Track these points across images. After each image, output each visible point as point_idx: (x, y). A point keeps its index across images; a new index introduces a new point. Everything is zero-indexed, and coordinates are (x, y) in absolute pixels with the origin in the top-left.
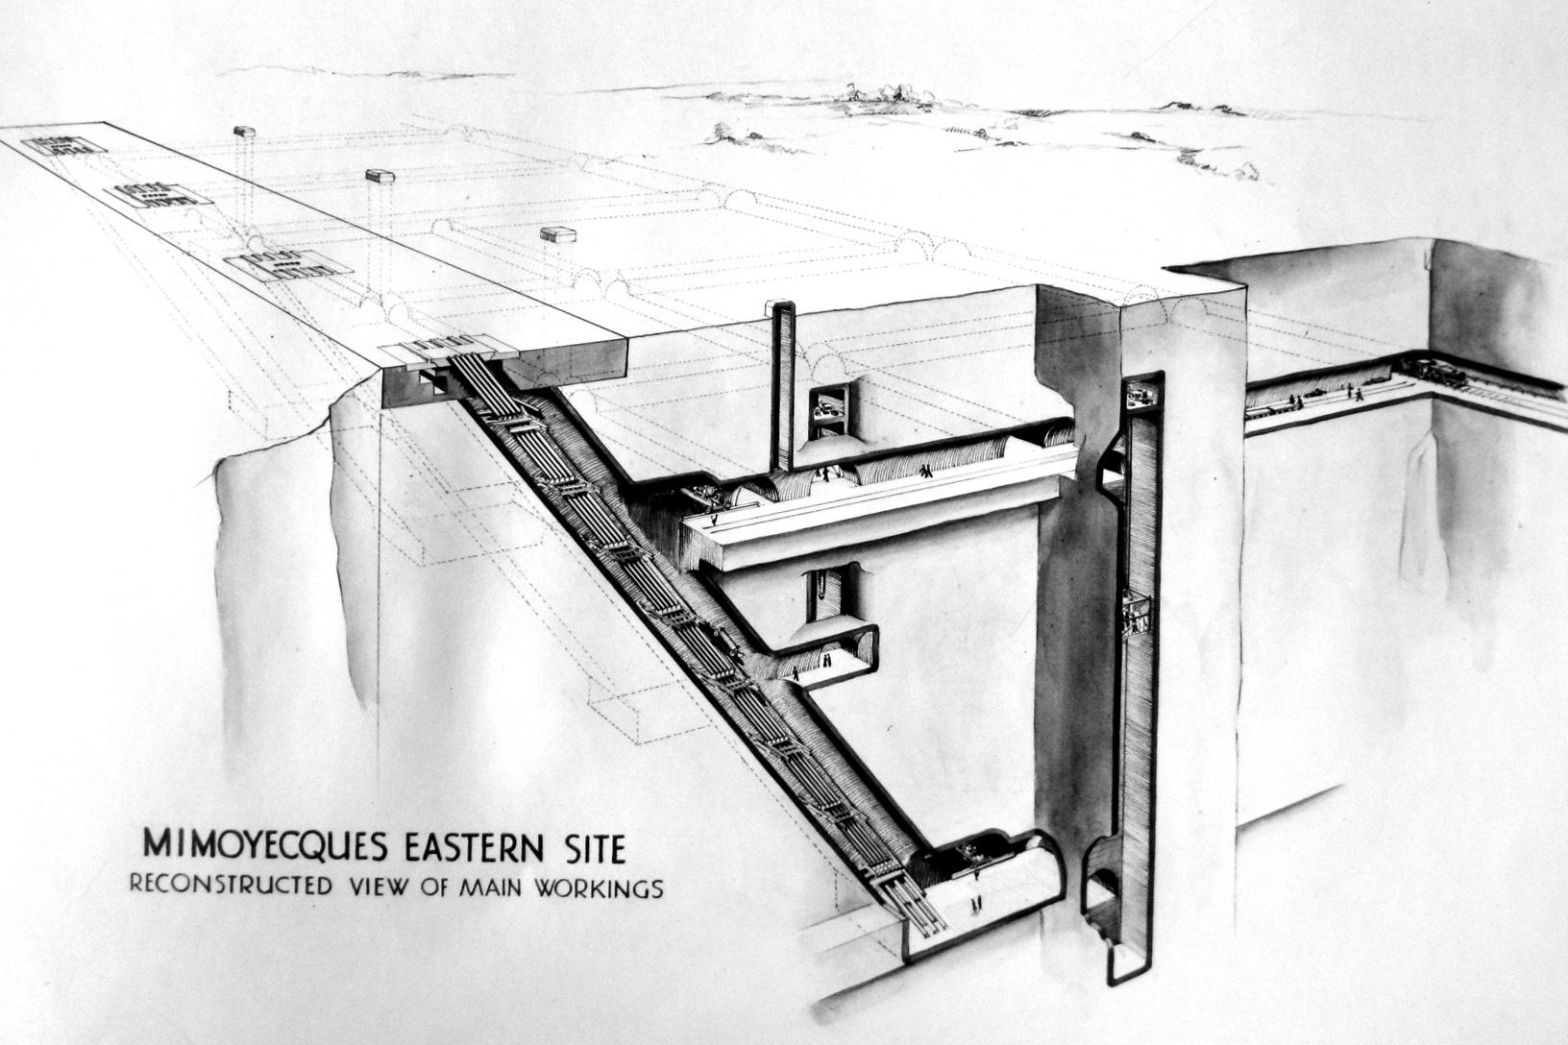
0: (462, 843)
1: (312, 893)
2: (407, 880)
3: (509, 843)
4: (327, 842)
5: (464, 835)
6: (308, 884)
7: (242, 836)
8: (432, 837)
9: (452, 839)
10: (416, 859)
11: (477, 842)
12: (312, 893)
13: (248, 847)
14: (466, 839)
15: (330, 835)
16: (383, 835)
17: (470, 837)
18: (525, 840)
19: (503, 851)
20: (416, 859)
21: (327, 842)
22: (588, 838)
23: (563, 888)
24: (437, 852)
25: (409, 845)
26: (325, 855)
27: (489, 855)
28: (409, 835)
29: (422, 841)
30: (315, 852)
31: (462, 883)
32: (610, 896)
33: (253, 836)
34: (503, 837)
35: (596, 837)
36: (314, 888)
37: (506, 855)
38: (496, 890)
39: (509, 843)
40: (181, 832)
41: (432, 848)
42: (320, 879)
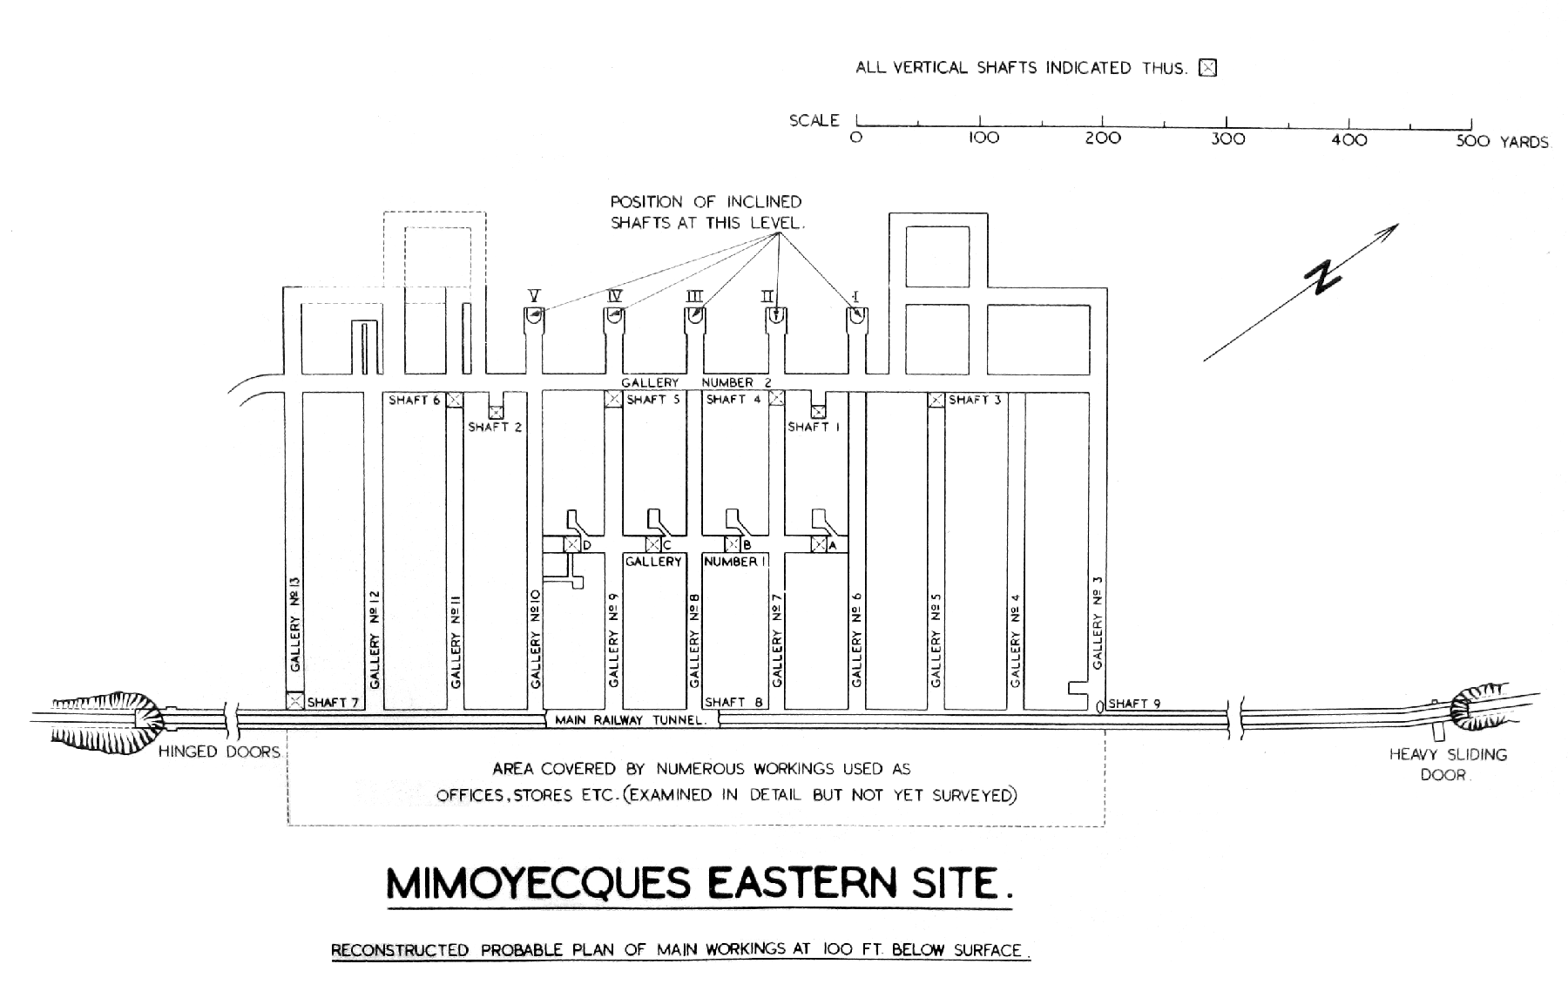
0: (791, 879)
2: (893, 870)
4: (615, 880)
5: (791, 869)
8: (748, 872)
11: (809, 877)
15: (619, 871)
16: (686, 871)
21: (615, 880)
22: (942, 870)
24: (754, 886)
27: (1114, 70)
29: (732, 882)
30: (601, 892)
33: (514, 873)
34: (845, 870)
37: (706, 771)
39: (293, 627)
40: (427, 870)
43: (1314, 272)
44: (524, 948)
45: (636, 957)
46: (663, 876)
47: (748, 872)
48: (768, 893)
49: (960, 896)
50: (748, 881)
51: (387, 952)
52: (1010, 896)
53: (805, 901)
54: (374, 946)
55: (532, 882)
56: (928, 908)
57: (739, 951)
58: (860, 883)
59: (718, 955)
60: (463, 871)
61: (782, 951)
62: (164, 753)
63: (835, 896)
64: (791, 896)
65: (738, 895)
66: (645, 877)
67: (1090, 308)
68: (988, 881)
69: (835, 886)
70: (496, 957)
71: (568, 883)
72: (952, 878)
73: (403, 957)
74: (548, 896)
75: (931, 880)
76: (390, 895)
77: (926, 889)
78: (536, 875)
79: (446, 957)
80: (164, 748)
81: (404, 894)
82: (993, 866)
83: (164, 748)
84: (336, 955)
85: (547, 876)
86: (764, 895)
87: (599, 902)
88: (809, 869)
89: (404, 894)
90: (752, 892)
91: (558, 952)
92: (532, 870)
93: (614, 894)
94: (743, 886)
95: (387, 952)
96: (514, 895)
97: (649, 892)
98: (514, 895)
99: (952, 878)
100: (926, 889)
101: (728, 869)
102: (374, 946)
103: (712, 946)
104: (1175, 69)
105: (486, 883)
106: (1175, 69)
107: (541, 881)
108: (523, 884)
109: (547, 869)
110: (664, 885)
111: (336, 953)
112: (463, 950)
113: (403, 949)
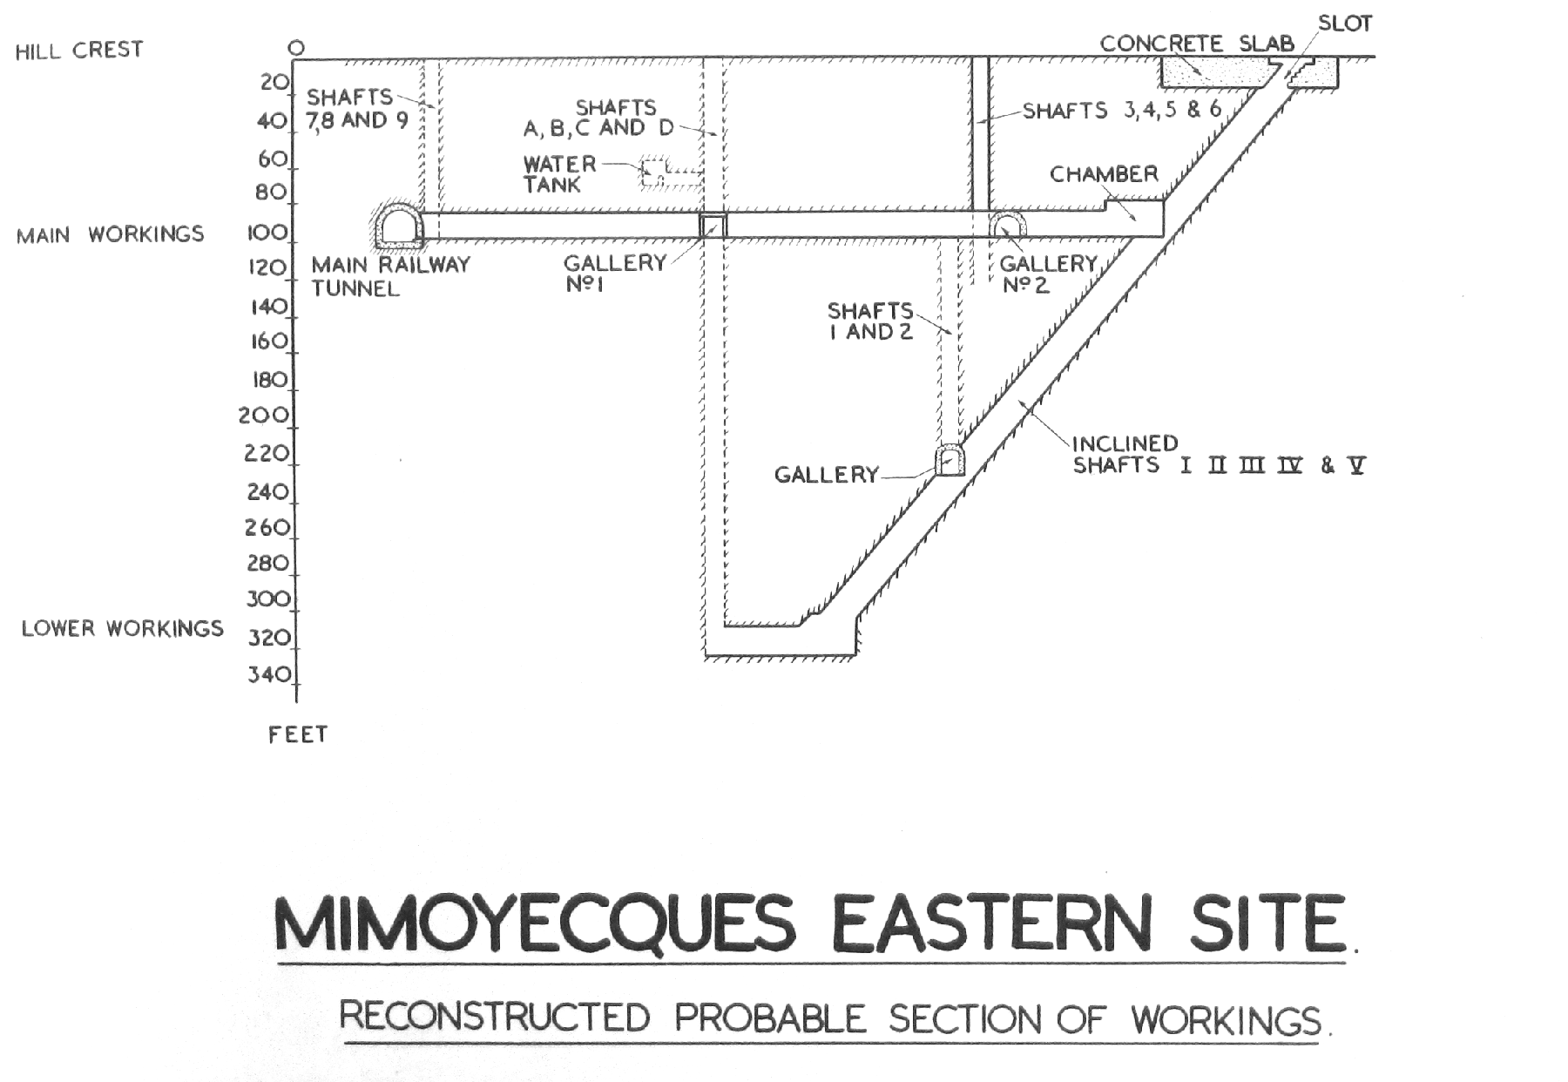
0: (971, 916)
5: (973, 898)
7: (473, 906)
8: (901, 903)
9: (944, 910)
13: (484, 925)
14: (981, 906)
22: (1244, 903)
23: (1174, 1020)
24: (912, 929)
25: (842, 920)
26: (666, 943)
29: (876, 916)
31: (784, 1008)
32: (156, 240)
35: (1265, 898)
37: (1077, 267)
38: (794, 1021)
42: (629, 1006)
44: (778, 1017)
45: (1083, 1035)
46: (747, 911)
47: (901, 903)
48: (936, 944)
49: (590, 1028)
50: (901, 919)
51: (465, 1018)
52: (1357, 951)
53: (996, 953)
54: (436, 1006)
55: (527, 921)
56: (1269, 963)
57: (1211, 1024)
58: (1087, 926)
59: (1159, 1035)
60: (410, 901)
61: (1314, 1027)
62: (23, 56)
63: (1048, 946)
64: (974, 946)
65: (882, 946)
66: (716, 913)
67: (1103, 211)
69: (1045, 930)
70: (710, 1032)
71: (591, 921)
72: (1262, 915)
73: (502, 1034)
74: (554, 948)
75: (1224, 918)
76: (281, 944)
77: (1215, 935)
78: (536, 910)
79: (599, 1033)
80: (23, 47)
81: (305, 941)
82: (546, 1007)
83: (23, 47)
84: (353, 1030)
85: (553, 911)
86: (928, 947)
87: (648, 955)
88: (1003, 898)
89: (305, 941)
90: (908, 940)
91: (855, 1024)
92: (528, 899)
93: (666, 943)
94: (890, 930)
95: (465, 1018)
96: (495, 946)
98: (495, 946)
99: (1262, 915)
100: (1215, 935)
101: (868, 899)
102: (436, 1006)
103: (1146, 1012)
107: (543, 921)
109: (552, 898)
110: (750, 928)
111: (349, 1021)
112: (638, 1018)
113: (501, 1010)
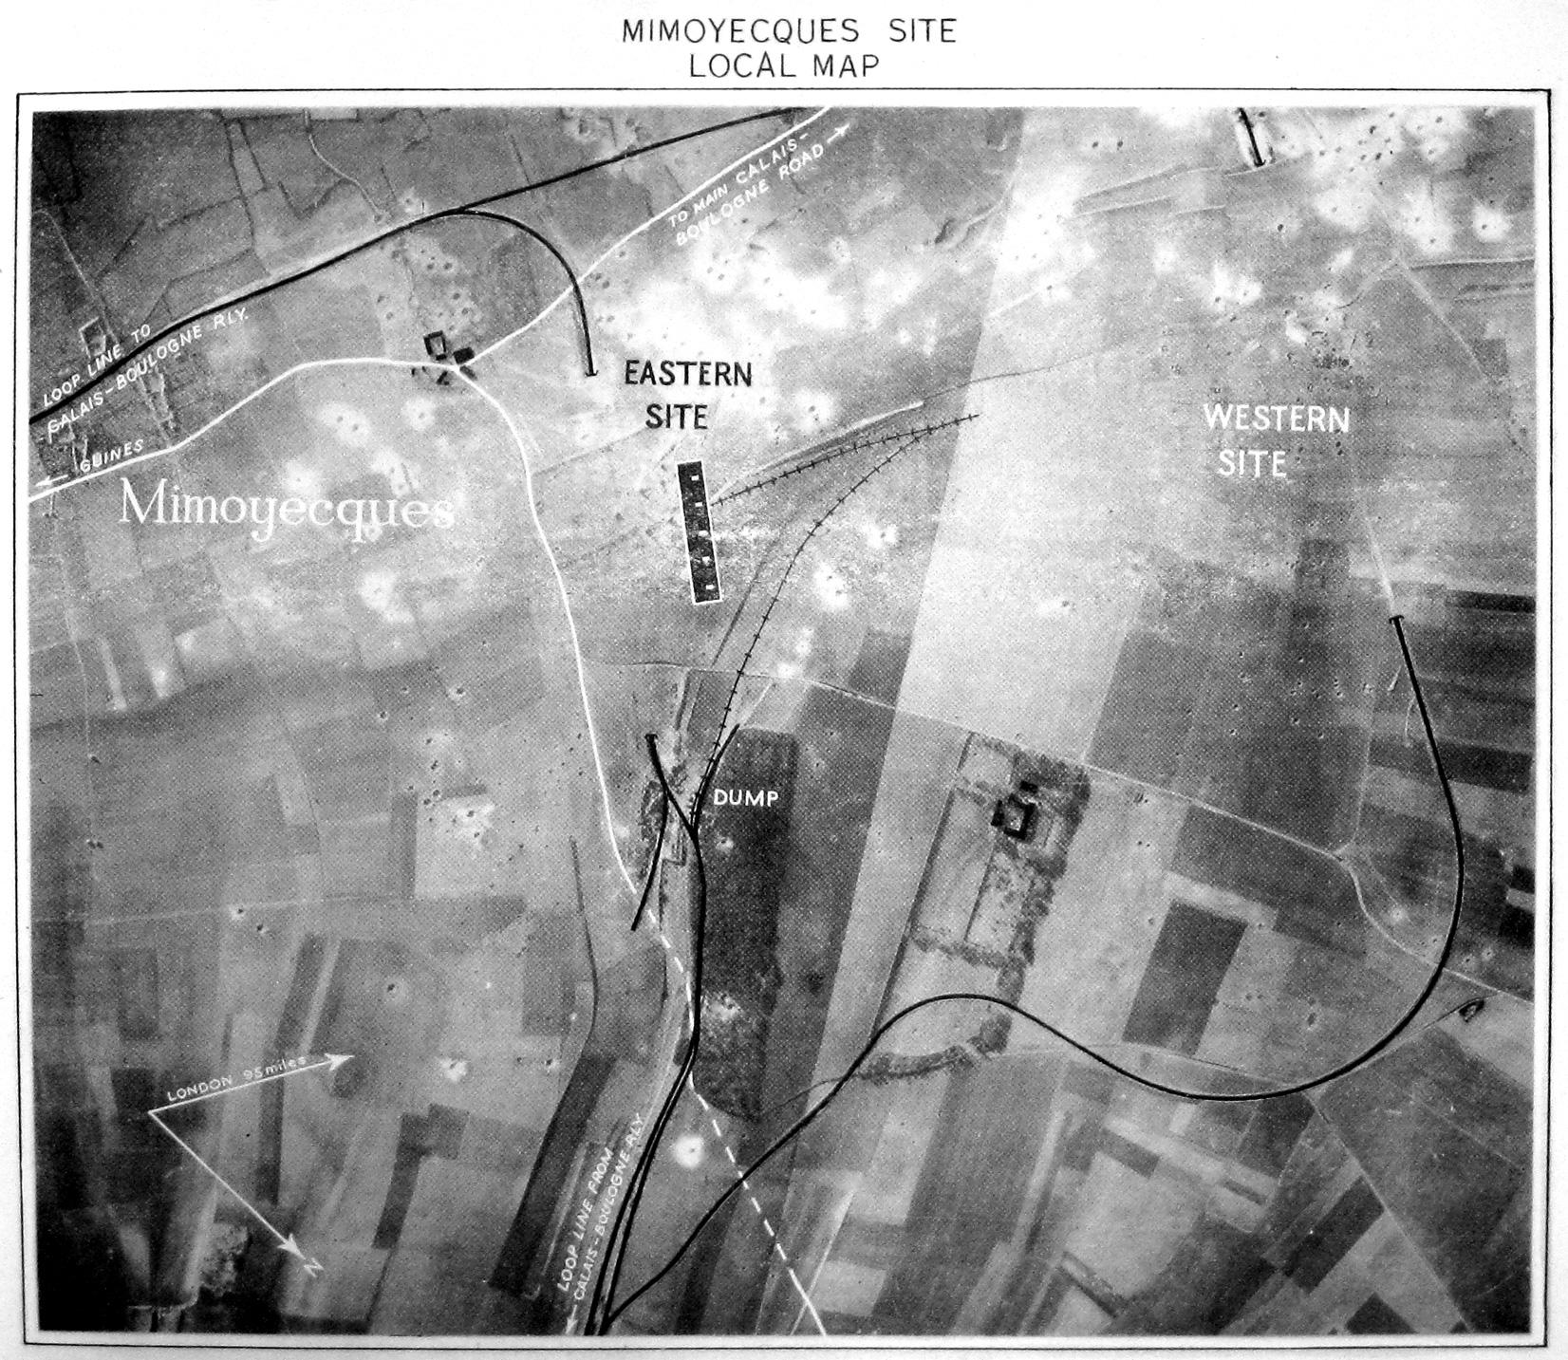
1: (708, 384)
2: (749, 365)
3: (723, 369)
5: (679, 363)
6: (703, 373)
8: (648, 365)
10: (635, 383)
12: (708, 384)
17: (687, 365)
18: (737, 367)
19: (718, 374)
20: (635, 383)
22: (669, 407)
24: (652, 376)
25: (629, 372)
28: (629, 363)
34: (718, 365)
36: (710, 377)
37: (721, 378)
39: (723, 369)
41: (648, 373)
43: (749, 372)
49: (717, 40)
52: (813, 312)
68: (703, 416)
97: (826, 38)
104: (663, 415)
105: (695, 31)
106: (663, 415)
108: (726, 31)
